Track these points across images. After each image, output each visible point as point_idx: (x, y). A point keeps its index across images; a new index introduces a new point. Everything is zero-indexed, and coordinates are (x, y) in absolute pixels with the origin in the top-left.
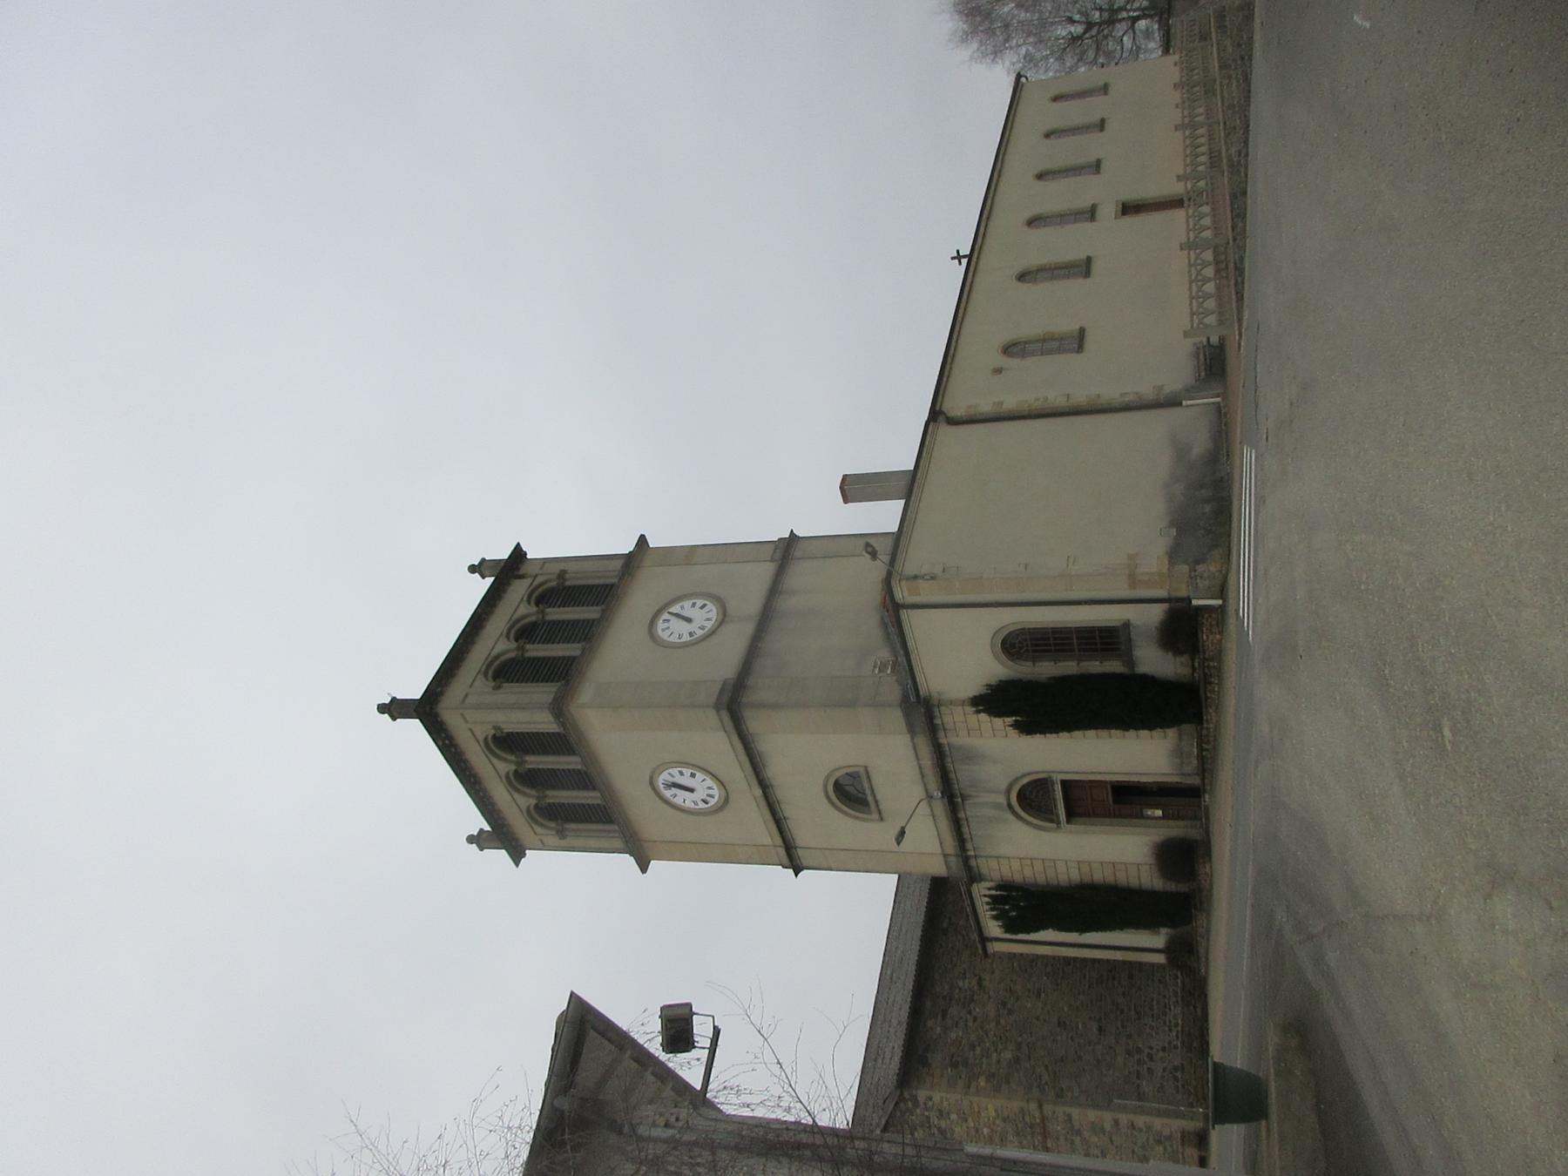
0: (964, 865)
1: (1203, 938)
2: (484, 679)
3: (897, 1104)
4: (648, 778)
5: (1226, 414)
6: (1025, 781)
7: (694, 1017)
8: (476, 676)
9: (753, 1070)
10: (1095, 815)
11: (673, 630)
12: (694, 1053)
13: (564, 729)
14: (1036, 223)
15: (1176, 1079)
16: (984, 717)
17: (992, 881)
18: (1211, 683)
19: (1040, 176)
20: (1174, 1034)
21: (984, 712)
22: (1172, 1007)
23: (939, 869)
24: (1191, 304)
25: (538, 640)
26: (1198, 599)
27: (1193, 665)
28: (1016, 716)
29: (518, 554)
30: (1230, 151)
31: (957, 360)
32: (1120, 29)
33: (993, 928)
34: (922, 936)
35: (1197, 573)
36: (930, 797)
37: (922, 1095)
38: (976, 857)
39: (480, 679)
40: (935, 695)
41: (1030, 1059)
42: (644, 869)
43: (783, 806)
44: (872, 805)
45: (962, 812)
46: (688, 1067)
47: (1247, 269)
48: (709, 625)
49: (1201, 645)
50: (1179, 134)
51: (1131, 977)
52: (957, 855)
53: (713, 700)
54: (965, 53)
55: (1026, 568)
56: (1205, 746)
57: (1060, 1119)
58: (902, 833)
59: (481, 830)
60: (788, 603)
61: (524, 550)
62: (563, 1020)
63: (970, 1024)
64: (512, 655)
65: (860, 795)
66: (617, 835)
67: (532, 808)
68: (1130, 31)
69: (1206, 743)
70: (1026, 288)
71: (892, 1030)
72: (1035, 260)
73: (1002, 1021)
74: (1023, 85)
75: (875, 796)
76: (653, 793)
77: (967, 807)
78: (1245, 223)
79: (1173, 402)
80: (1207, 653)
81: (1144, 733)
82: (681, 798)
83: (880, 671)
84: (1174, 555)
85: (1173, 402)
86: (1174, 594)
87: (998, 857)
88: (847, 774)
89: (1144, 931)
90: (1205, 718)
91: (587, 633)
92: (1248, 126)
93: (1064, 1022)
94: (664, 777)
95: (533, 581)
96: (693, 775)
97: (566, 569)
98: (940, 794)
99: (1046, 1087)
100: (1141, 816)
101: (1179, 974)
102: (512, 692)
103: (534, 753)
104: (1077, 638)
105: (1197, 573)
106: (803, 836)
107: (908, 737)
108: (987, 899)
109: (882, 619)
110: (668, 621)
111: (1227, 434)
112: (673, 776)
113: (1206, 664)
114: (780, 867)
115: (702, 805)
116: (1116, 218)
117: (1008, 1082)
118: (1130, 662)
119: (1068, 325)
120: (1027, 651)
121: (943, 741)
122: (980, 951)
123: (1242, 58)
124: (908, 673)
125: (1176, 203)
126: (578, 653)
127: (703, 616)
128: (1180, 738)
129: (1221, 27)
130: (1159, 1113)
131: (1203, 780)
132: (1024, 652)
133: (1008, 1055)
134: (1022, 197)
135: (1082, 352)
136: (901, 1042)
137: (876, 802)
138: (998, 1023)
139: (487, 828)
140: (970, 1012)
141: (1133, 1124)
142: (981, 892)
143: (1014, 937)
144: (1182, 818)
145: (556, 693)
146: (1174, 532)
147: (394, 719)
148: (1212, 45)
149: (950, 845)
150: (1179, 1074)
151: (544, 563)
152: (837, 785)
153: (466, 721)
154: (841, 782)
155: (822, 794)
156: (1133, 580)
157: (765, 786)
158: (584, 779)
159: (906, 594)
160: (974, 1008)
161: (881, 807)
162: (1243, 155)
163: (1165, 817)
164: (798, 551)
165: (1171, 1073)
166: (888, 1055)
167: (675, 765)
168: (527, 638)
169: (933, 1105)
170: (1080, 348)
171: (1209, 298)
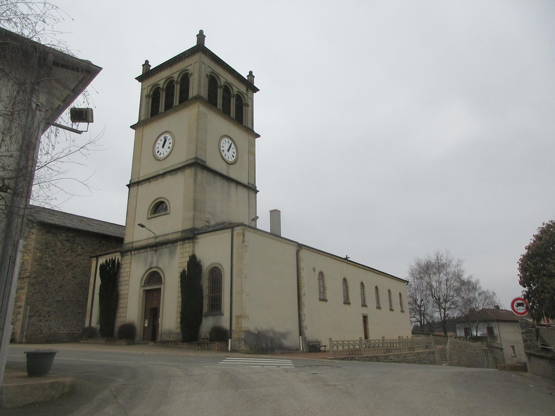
0: (128, 250)
1: (95, 342)
2: (210, 71)
3: (31, 220)
4: (170, 131)
5: (296, 352)
6: (161, 274)
7: (87, 123)
8: (211, 68)
9: (67, 139)
10: (146, 300)
11: (225, 144)
12: (70, 122)
13: (190, 100)
14: (362, 286)
15: (37, 331)
16: (188, 259)
17: (121, 260)
18: (198, 346)
19: (376, 288)
20: (56, 330)
21: (190, 259)
22: (67, 329)
23: (127, 240)
24: (352, 341)
25: (224, 93)
26: (231, 341)
27: (205, 339)
28: (188, 271)
29: (256, 90)
30: (391, 356)
31: (318, 255)
32: (418, 317)
33: (102, 261)
34: (99, 233)
35: (241, 341)
36: (156, 238)
37: (34, 231)
38: (131, 254)
39: (211, 70)
40: (197, 241)
41: (47, 273)
42: (132, 127)
43: (155, 181)
44: (154, 215)
45: (149, 250)
46: (65, 118)
47: (352, 362)
48: (226, 158)
49: (213, 342)
50: (381, 338)
51: (79, 313)
52: (132, 247)
53: (199, 156)
54: (413, 264)
55: (245, 277)
56: (173, 343)
57: (22, 285)
58: (143, 226)
59: (150, 66)
60: (233, 186)
61: (257, 92)
62: (89, 63)
63: (63, 250)
64: (219, 83)
65: (158, 211)
66: (146, 117)
67: (159, 86)
68: (417, 321)
69: (174, 343)
70: (341, 281)
71: (61, 220)
72: (350, 284)
73: (63, 263)
74: (405, 283)
75: (157, 216)
76: (160, 133)
77: (152, 252)
78: (368, 361)
79: (301, 333)
80: (210, 345)
81: (179, 320)
82: (160, 142)
83: (206, 220)
84: (248, 332)
85: (301, 333)
86: (233, 332)
87: (131, 263)
88: (167, 206)
89: (98, 319)
90: (184, 343)
91: (225, 112)
92: (400, 362)
93: (62, 287)
94: (169, 137)
95: (245, 94)
96: (169, 148)
97: (249, 107)
98: (157, 241)
99: (36, 279)
100: (145, 318)
101: (80, 332)
102: (205, 82)
103: (180, 88)
104: (217, 296)
105: (241, 341)
106: (142, 189)
107: (181, 230)
108: (114, 258)
109: (226, 223)
110: (229, 143)
111: (290, 353)
112: (169, 140)
113: (206, 344)
114: (130, 179)
115: (157, 151)
116: (362, 314)
117: (38, 265)
118: (207, 315)
119: (328, 296)
120: (213, 276)
121: (179, 243)
122: (93, 255)
123: (420, 360)
124: (205, 231)
125: (366, 337)
126: (218, 107)
127: (230, 156)
128: (178, 334)
129: (429, 353)
130: (23, 325)
131: (160, 342)
132: (213, 275)
133: (50, 265)
134: (371, 280)
135: (319, 300)
136: (57, 223)
137: (155, 217)
138: (63, 261)
139: (151, 68)
140: (67, 250)
141: (19, 313)
142: (117, 256)
143: (98, 268)
144: (144, 333)
145: (204, 98)
146: (256, 333)
147: (197, 36)
148: (424, 350)
149: (136, 245)
150: (39, 332)
151: (252, 99)
152: (162, 202)
153: (195, 63)
154: (164, 204)
155: (162, 196)
156: (239, 317)
157: (164, 175)
158: (169, 106)
159: (237, 231)
160: (69, 252)
161: (153, 219)
162: (390, 361)
163: (144, 327)
164: (251, 193)
165: (40, 329)
166: (51, 218)
167: (174, 141)
168: (225, 90)
169: (30, 235)
170: (320, 300)
171: (343, 347)
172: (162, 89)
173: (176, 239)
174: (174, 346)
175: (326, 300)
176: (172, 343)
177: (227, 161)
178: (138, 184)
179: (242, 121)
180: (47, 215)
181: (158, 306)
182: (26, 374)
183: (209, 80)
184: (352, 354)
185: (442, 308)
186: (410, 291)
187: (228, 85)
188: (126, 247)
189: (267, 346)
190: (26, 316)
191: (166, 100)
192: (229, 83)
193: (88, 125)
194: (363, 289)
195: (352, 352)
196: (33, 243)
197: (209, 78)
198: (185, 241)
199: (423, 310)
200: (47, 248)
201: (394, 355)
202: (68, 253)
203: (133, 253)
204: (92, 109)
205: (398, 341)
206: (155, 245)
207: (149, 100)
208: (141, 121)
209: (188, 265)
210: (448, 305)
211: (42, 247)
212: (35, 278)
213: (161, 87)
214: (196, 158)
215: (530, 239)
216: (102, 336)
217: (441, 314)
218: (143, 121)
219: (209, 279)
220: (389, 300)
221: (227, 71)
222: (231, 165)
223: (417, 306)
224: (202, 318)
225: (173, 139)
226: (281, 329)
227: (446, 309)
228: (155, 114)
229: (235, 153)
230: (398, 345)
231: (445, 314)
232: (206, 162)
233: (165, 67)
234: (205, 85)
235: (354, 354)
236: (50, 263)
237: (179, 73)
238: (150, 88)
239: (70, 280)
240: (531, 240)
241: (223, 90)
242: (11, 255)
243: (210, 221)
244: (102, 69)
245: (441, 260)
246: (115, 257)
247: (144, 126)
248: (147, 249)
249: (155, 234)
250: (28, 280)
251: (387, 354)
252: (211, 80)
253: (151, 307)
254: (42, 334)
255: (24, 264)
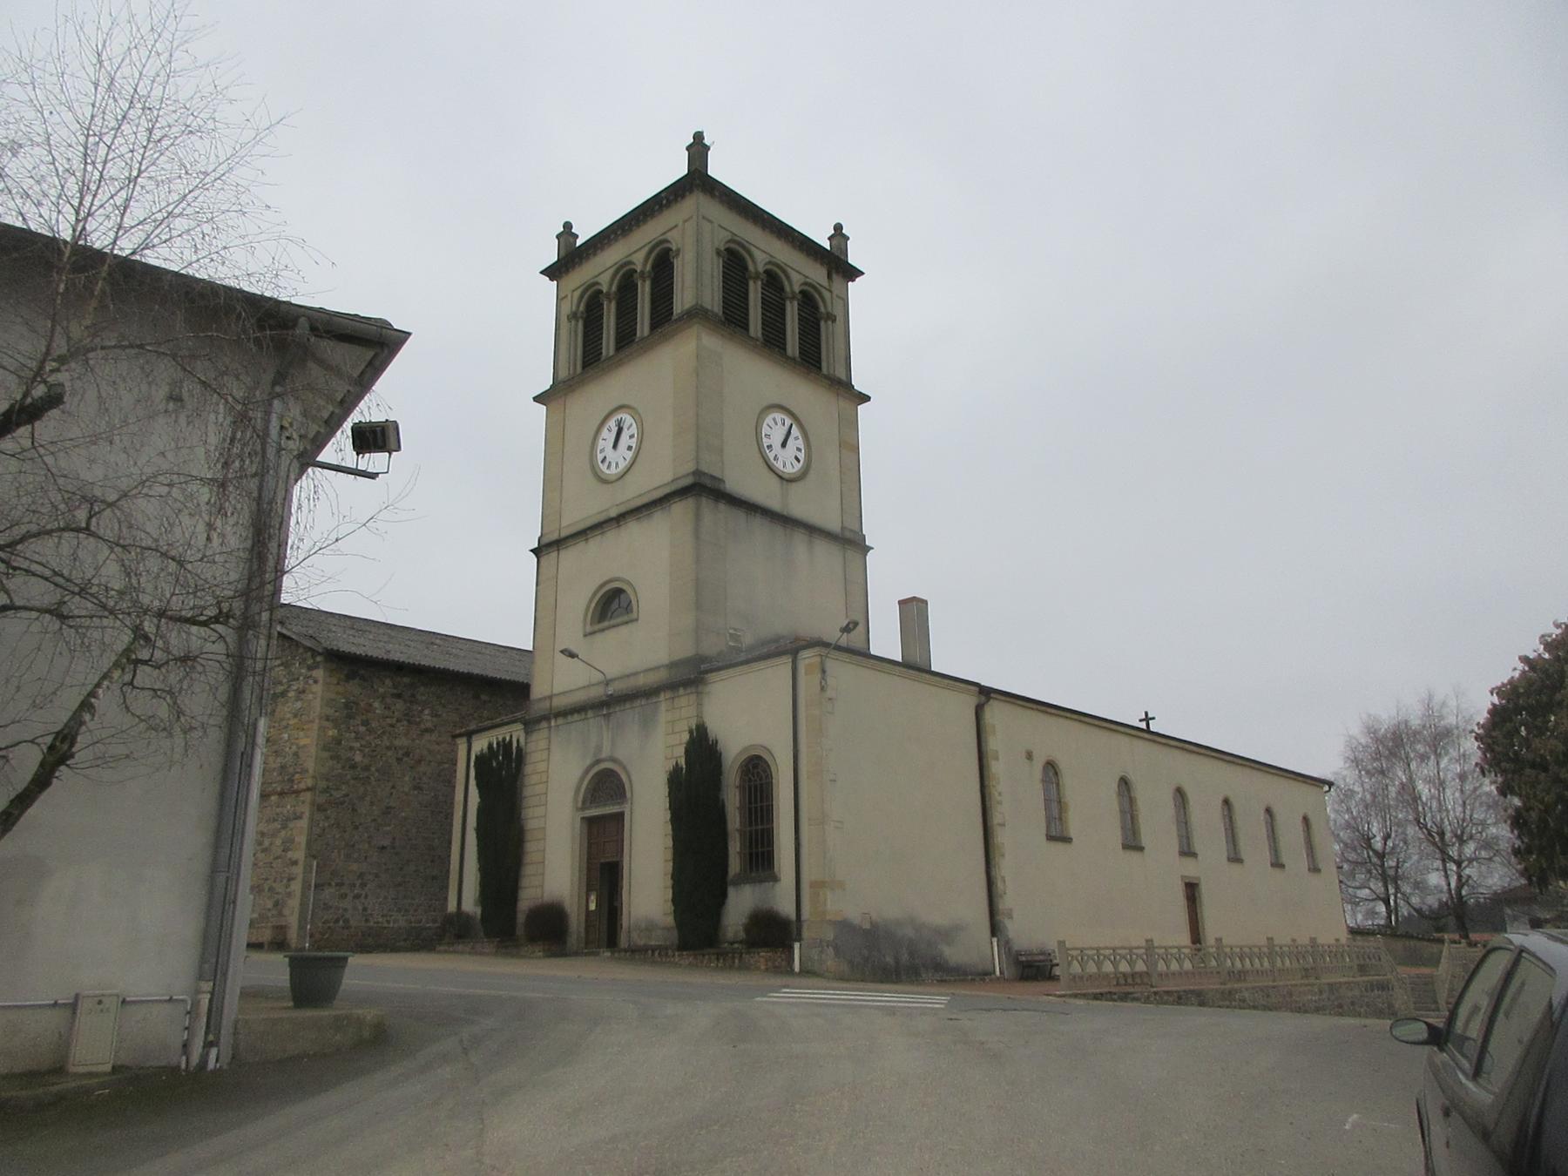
3: (310, 649)
6: (624, 777)
7: (387, 454)
11: (774, 428)
15: (337, 921)
16: (686, 737)
17: (526, 743)
18: (718, 959)
19: (1226, 802)
20: (380, 920)
23: (538, 691)
27: (737, 942)
29: (853, 273)
33: (480, 744)
36: (607, 683)
37: (319, 673)
38: (550, 728)
39: (728, 236)
42: (537, 399)
43: (599, 537)
46: (339, 448)
48: (779, 465)
51: (434, 878)
53: (705, 468)
54: (1356, 730)
58: (572, 655)
59: (577, 236)
61: (857, 279)
62: (383, 325)
63: (389, 721)
64: (751, 268)
65: (610, 614)
68: (1375, 897)
72: (1141, 793)
73: (389, 753)
79: (995, 929)
80: (747, 956)
81: (670, 895)
82: (608, 436)
84: (844, 926)
87: (549, 749)
88: (631, 602)
90: (685, 953)
91: (773, 342)
94: (628, 419)
95: (825, 288)
96: (630, 448)
98: (610, 693)
100: (589, 890)
102: (713, 269)
104: (763, 830)
106: (569, 558)
107: (667, 662)
108: (508, 739)
115: (600, 457)
119: (1074, 827)
121: (662, 697)
123: (1340, 1006)
126: (752, 332)
127: (788, 460)
129: (1372, 987)
130: (303, 905)
131: (626, 951)
133: (358, 758)
135: (1047, 839)
138: (388, 748)
139: (579, 242)
140: (398, 721)
142: (515, 733)
143: (472, 764)
146: (867, 926)
147: (688, 149)
149: (559, 703)
152: (618, 592)
153: (685, 221)
156: (818, 885)
157: (620, 519)
158: (626, 338)
159: (807, 661)
162: (1241, 1003)
164: (851, 554)
172: (608, 294)
173: (655, 686)
174: (659, 960)
175: (1067, 840)
176: (653, 952)
177: (781, 474)
178: (558, 547)
179: (819, 361)
180: (347, 632)
181: (618, 860)
182: (291, 1004)
183: (724, 262)
184: (1125, 985)
185: (1451, 859)
186: (1349, 810)
187: (775, 269)
188: (537, 709)
189: (897, 962)
190: (310, 885)
191: (617, 324)
192: (779, 262)
193: (390, 457)
194: (1185, 808)
195: (1126, 981)
196: (317, 704)
197: (723, 257)
198: (678, 691)
199: (1394, 864)
200: (350, 717)
201: (1253, 988)
202: (401, 728)
203: (553, 723)
204: (395, 422)
205: (1265, 950)
206: (603, 701)
207: (577, 325)
208: (559, 383)
209: (687, 752)
210: (1470, 849)
211: (337, 714)
212: (326, 790)
213: (604, 291)
214: (697, 473)
215: (1513, 666)
216: (488, 935)
217: (1447, 876)
218: (564, 382)
219: (741, 788)
220: (1268, 836)
221: (772, 232)
222: (794, 484)
223: (1371, 853)
224: (726, 888)
225: (639, 424)
226: (936, 917)
227: (1463, 862)
228: (592, 363)
229: (803, 451)
230: (1266, 964)
231: (1460, 877)
232: (724, 482)
233: (612, 236)
234: (712, 277)
235: (1130, 985)
236: (358, 752)
237: (647, 249)
238: (577, 294)
239: (406, 794)
240: (1515, 669)
241: (762, 283)
242: (243, 750)
243: (739, 636)
244: (409, 334)
245: (1441, 717)
246: (509, 734)
247: (566, 395)
248: (586, 714)
249: (602, 673)
250: (308, 796)
251: (1229, 986)
252: (728, 262)
253: (602, 861)
254: (347, 928)
255: (298, 757)
